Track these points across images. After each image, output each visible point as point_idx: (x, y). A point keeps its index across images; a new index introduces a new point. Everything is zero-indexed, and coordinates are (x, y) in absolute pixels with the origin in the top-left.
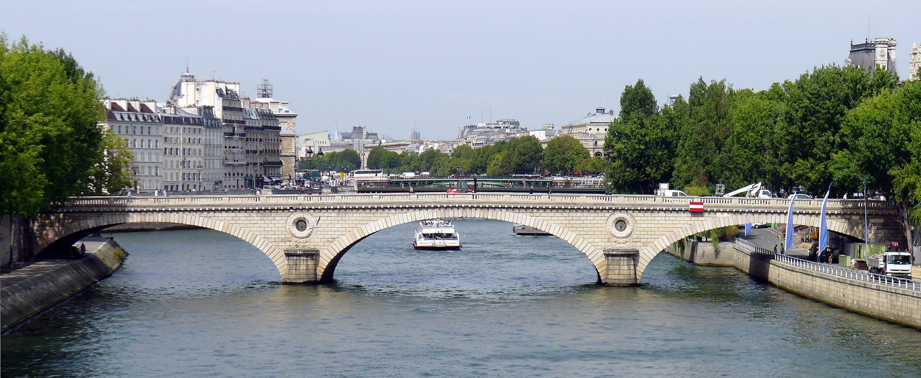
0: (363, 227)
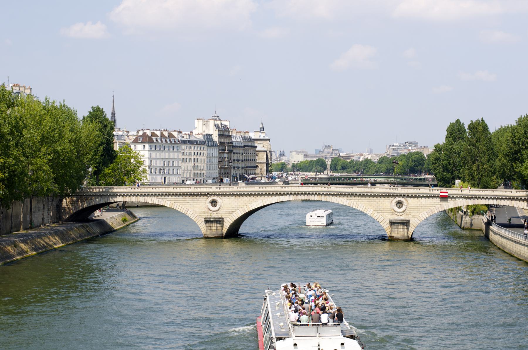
0: (249, 205)
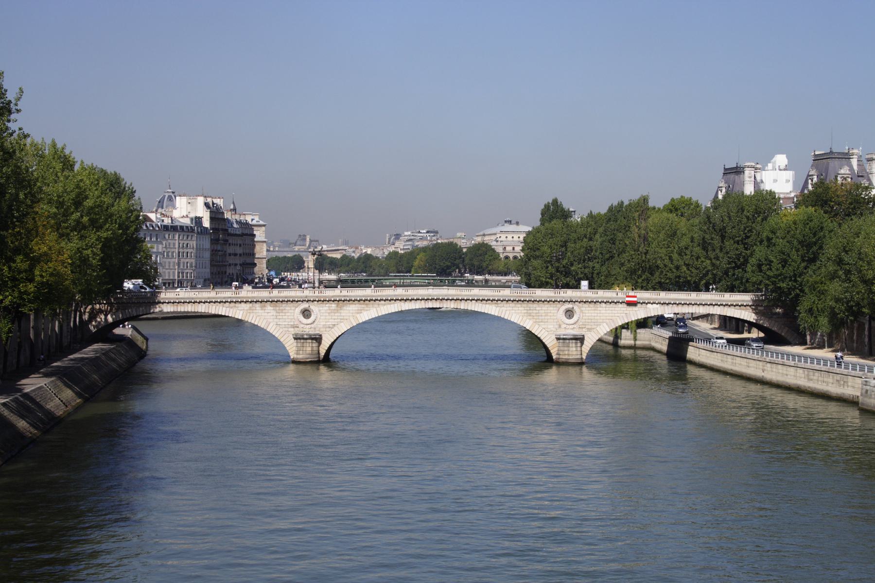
0: (358, 316)
